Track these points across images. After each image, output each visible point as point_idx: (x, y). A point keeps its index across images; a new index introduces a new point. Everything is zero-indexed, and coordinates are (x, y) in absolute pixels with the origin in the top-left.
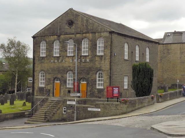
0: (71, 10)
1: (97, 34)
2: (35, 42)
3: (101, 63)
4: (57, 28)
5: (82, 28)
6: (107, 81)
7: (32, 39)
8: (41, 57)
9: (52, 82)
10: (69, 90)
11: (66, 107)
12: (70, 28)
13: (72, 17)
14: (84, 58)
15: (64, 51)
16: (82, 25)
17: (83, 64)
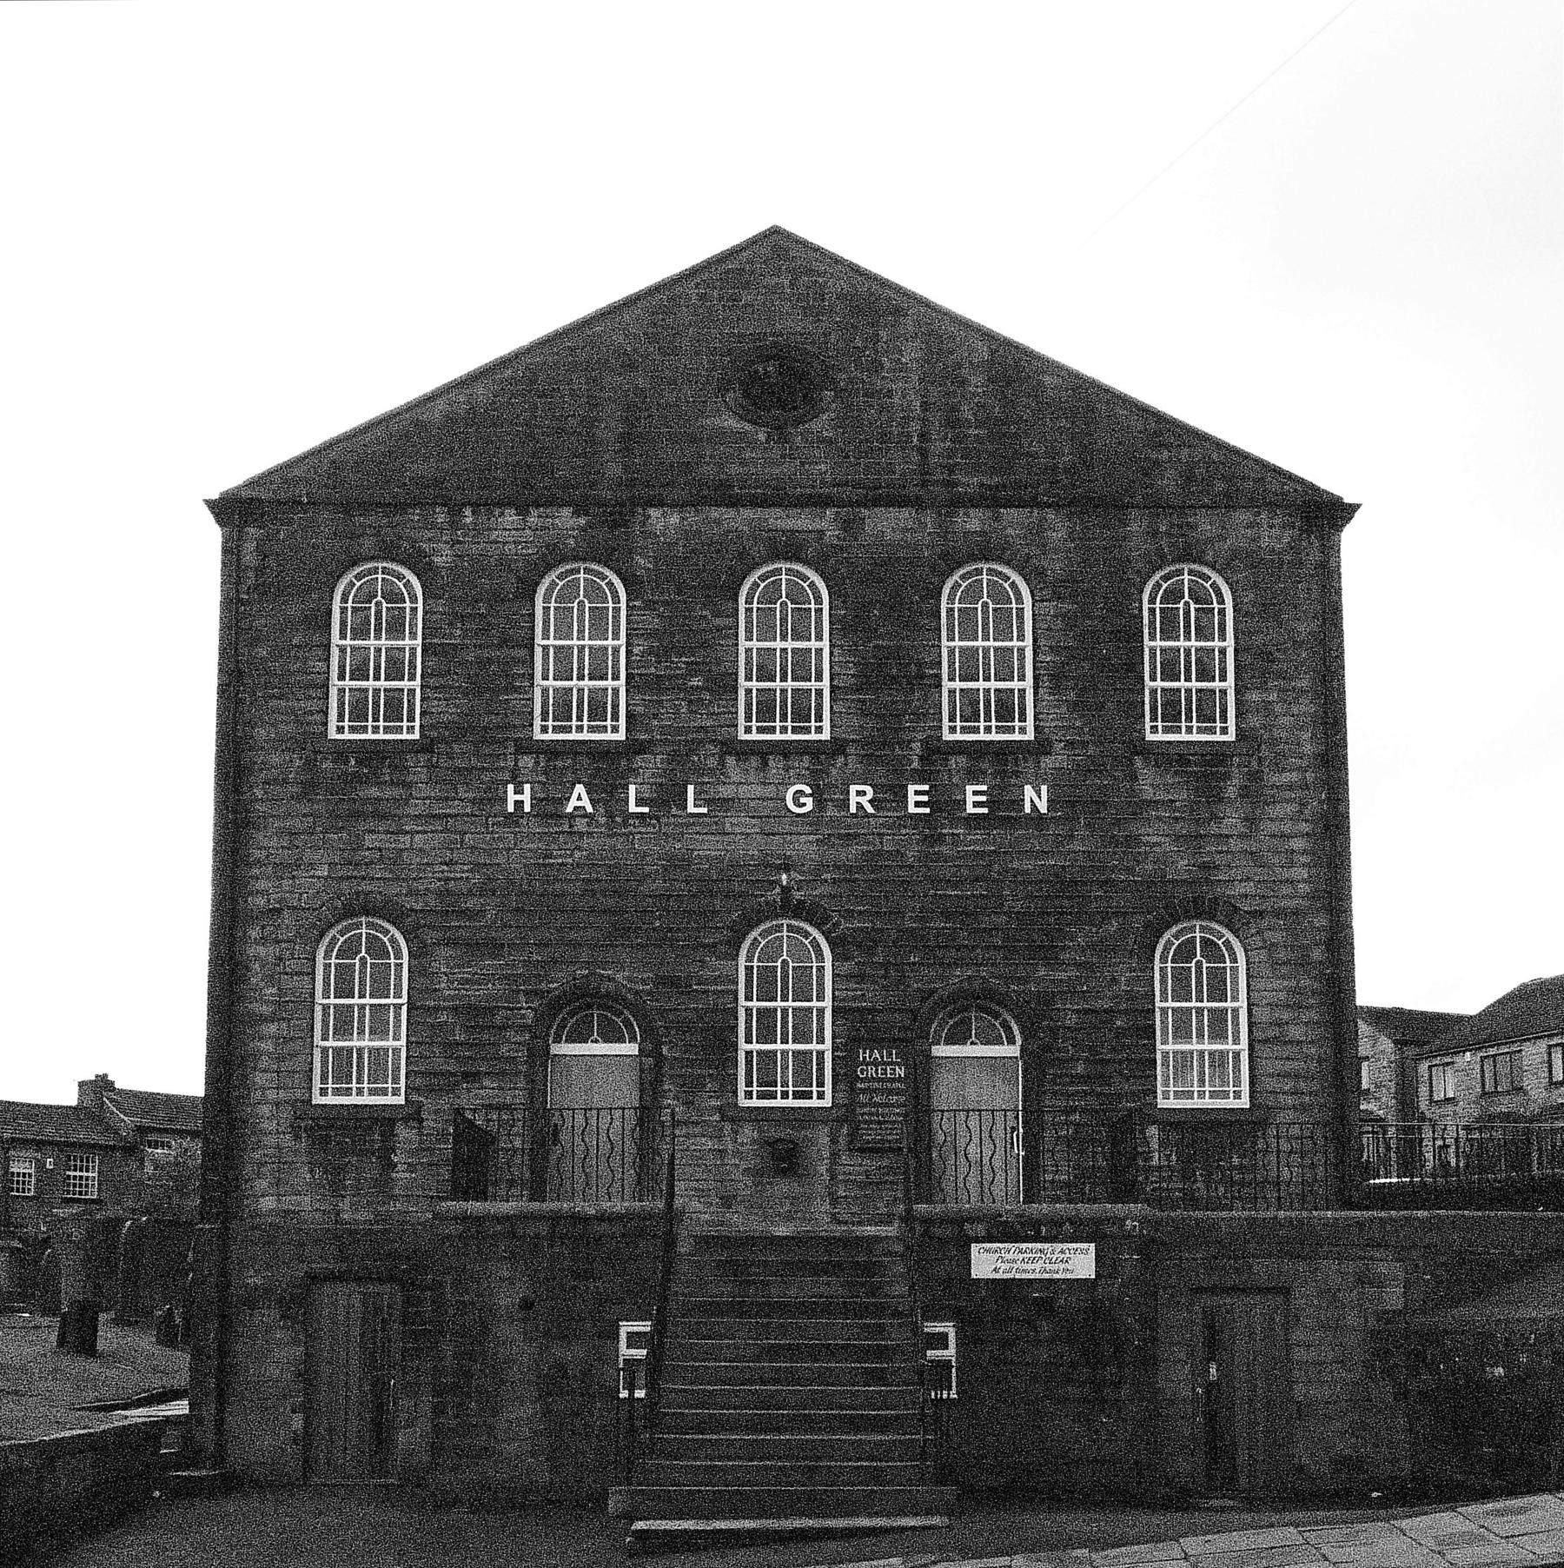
0: (775, 231)
1: (1136, 525)
2: (260, 571)
3: (1214, 829)
4: (590, 423)
5: (937, 446)
6: (1295, 1032)
7: (212, 536)
8: (342, 751)
9: (513, 1046)
10: (786, 1133)
11: (957, 1315)
12: (779, 432)
13: (793, 324)
14: (973, 776)
15: (696, 682)
16: (936, 418)
17: (975, 840)
